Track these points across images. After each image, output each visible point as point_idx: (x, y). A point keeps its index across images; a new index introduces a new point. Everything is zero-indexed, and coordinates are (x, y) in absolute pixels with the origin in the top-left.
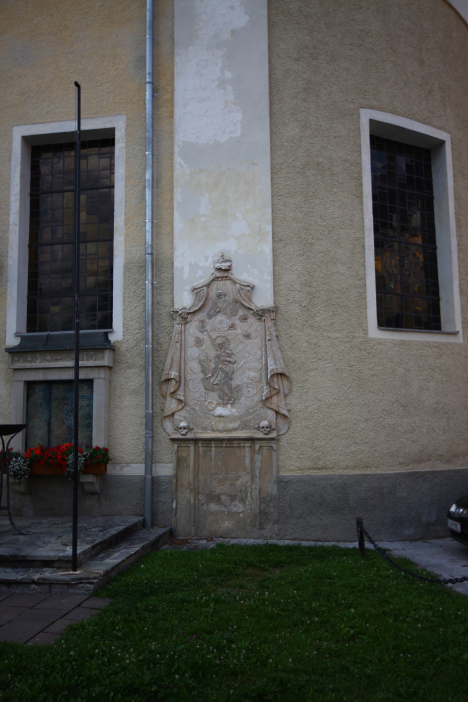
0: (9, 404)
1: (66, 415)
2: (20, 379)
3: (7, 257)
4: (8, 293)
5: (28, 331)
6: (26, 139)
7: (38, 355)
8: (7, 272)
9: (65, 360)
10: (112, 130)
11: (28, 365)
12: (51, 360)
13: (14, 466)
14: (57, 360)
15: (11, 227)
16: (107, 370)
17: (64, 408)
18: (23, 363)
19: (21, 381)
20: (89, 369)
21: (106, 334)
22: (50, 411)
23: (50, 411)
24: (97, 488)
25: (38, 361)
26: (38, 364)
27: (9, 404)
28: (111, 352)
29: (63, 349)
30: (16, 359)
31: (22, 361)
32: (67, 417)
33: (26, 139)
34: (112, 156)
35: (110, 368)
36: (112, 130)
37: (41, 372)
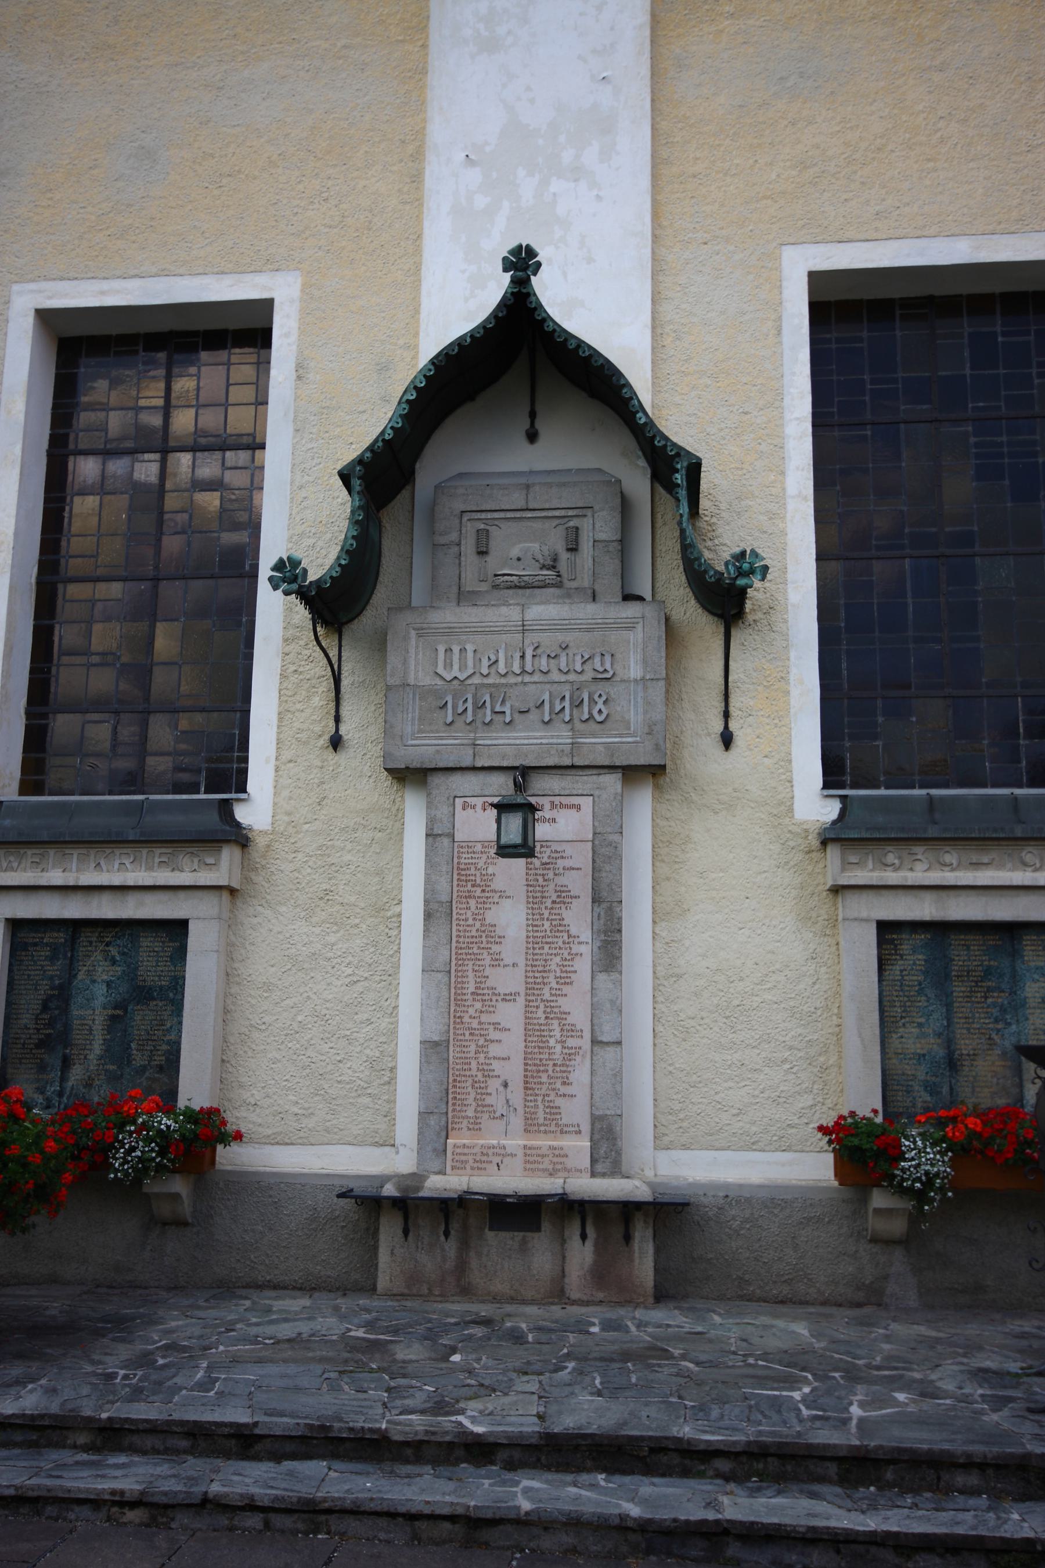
0: (814, 983)
1: (996, 1021)
2: (864, 914)
3: (785, 582)
4: (792, 678)
5: (22, 793)
6: (45, 317)
7: (919, 850)
8: (786, 621)
9: (1001, 867)
10: (267, 306)
11: (892, 877)
12: (959, 867)
13: (919, 1165)
14: (976, 865)
15: (791, 505)
16: (225, 895)
17: (990, 1000)
18: (872, 870)
19: (866, 920)
20: (871, 893)
21: (226, 809)
22: (949, 1006)
23: (949, 1006)
24: (186, 1208)
25: (919, 866)
26: (56, 877)
27: (814, 983)
28: (237, 851)
29: (1002, 835)
30: (853, 859)
31: (870, 865)
32: (1000, 1026)
33: (45, 317)
34: (263, 365)
35: (232, 891)
36: (267, 306)
37: (928, 897)
